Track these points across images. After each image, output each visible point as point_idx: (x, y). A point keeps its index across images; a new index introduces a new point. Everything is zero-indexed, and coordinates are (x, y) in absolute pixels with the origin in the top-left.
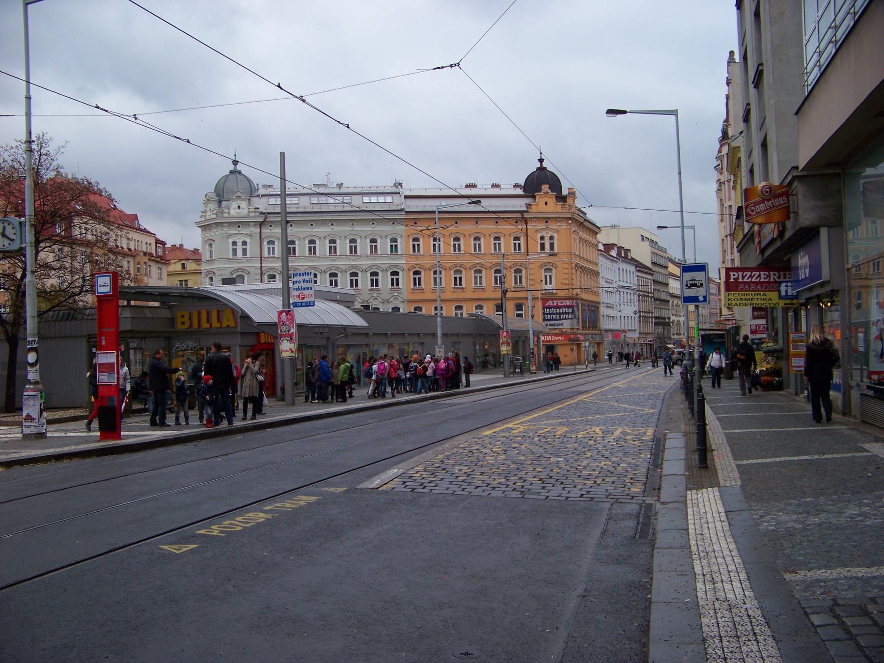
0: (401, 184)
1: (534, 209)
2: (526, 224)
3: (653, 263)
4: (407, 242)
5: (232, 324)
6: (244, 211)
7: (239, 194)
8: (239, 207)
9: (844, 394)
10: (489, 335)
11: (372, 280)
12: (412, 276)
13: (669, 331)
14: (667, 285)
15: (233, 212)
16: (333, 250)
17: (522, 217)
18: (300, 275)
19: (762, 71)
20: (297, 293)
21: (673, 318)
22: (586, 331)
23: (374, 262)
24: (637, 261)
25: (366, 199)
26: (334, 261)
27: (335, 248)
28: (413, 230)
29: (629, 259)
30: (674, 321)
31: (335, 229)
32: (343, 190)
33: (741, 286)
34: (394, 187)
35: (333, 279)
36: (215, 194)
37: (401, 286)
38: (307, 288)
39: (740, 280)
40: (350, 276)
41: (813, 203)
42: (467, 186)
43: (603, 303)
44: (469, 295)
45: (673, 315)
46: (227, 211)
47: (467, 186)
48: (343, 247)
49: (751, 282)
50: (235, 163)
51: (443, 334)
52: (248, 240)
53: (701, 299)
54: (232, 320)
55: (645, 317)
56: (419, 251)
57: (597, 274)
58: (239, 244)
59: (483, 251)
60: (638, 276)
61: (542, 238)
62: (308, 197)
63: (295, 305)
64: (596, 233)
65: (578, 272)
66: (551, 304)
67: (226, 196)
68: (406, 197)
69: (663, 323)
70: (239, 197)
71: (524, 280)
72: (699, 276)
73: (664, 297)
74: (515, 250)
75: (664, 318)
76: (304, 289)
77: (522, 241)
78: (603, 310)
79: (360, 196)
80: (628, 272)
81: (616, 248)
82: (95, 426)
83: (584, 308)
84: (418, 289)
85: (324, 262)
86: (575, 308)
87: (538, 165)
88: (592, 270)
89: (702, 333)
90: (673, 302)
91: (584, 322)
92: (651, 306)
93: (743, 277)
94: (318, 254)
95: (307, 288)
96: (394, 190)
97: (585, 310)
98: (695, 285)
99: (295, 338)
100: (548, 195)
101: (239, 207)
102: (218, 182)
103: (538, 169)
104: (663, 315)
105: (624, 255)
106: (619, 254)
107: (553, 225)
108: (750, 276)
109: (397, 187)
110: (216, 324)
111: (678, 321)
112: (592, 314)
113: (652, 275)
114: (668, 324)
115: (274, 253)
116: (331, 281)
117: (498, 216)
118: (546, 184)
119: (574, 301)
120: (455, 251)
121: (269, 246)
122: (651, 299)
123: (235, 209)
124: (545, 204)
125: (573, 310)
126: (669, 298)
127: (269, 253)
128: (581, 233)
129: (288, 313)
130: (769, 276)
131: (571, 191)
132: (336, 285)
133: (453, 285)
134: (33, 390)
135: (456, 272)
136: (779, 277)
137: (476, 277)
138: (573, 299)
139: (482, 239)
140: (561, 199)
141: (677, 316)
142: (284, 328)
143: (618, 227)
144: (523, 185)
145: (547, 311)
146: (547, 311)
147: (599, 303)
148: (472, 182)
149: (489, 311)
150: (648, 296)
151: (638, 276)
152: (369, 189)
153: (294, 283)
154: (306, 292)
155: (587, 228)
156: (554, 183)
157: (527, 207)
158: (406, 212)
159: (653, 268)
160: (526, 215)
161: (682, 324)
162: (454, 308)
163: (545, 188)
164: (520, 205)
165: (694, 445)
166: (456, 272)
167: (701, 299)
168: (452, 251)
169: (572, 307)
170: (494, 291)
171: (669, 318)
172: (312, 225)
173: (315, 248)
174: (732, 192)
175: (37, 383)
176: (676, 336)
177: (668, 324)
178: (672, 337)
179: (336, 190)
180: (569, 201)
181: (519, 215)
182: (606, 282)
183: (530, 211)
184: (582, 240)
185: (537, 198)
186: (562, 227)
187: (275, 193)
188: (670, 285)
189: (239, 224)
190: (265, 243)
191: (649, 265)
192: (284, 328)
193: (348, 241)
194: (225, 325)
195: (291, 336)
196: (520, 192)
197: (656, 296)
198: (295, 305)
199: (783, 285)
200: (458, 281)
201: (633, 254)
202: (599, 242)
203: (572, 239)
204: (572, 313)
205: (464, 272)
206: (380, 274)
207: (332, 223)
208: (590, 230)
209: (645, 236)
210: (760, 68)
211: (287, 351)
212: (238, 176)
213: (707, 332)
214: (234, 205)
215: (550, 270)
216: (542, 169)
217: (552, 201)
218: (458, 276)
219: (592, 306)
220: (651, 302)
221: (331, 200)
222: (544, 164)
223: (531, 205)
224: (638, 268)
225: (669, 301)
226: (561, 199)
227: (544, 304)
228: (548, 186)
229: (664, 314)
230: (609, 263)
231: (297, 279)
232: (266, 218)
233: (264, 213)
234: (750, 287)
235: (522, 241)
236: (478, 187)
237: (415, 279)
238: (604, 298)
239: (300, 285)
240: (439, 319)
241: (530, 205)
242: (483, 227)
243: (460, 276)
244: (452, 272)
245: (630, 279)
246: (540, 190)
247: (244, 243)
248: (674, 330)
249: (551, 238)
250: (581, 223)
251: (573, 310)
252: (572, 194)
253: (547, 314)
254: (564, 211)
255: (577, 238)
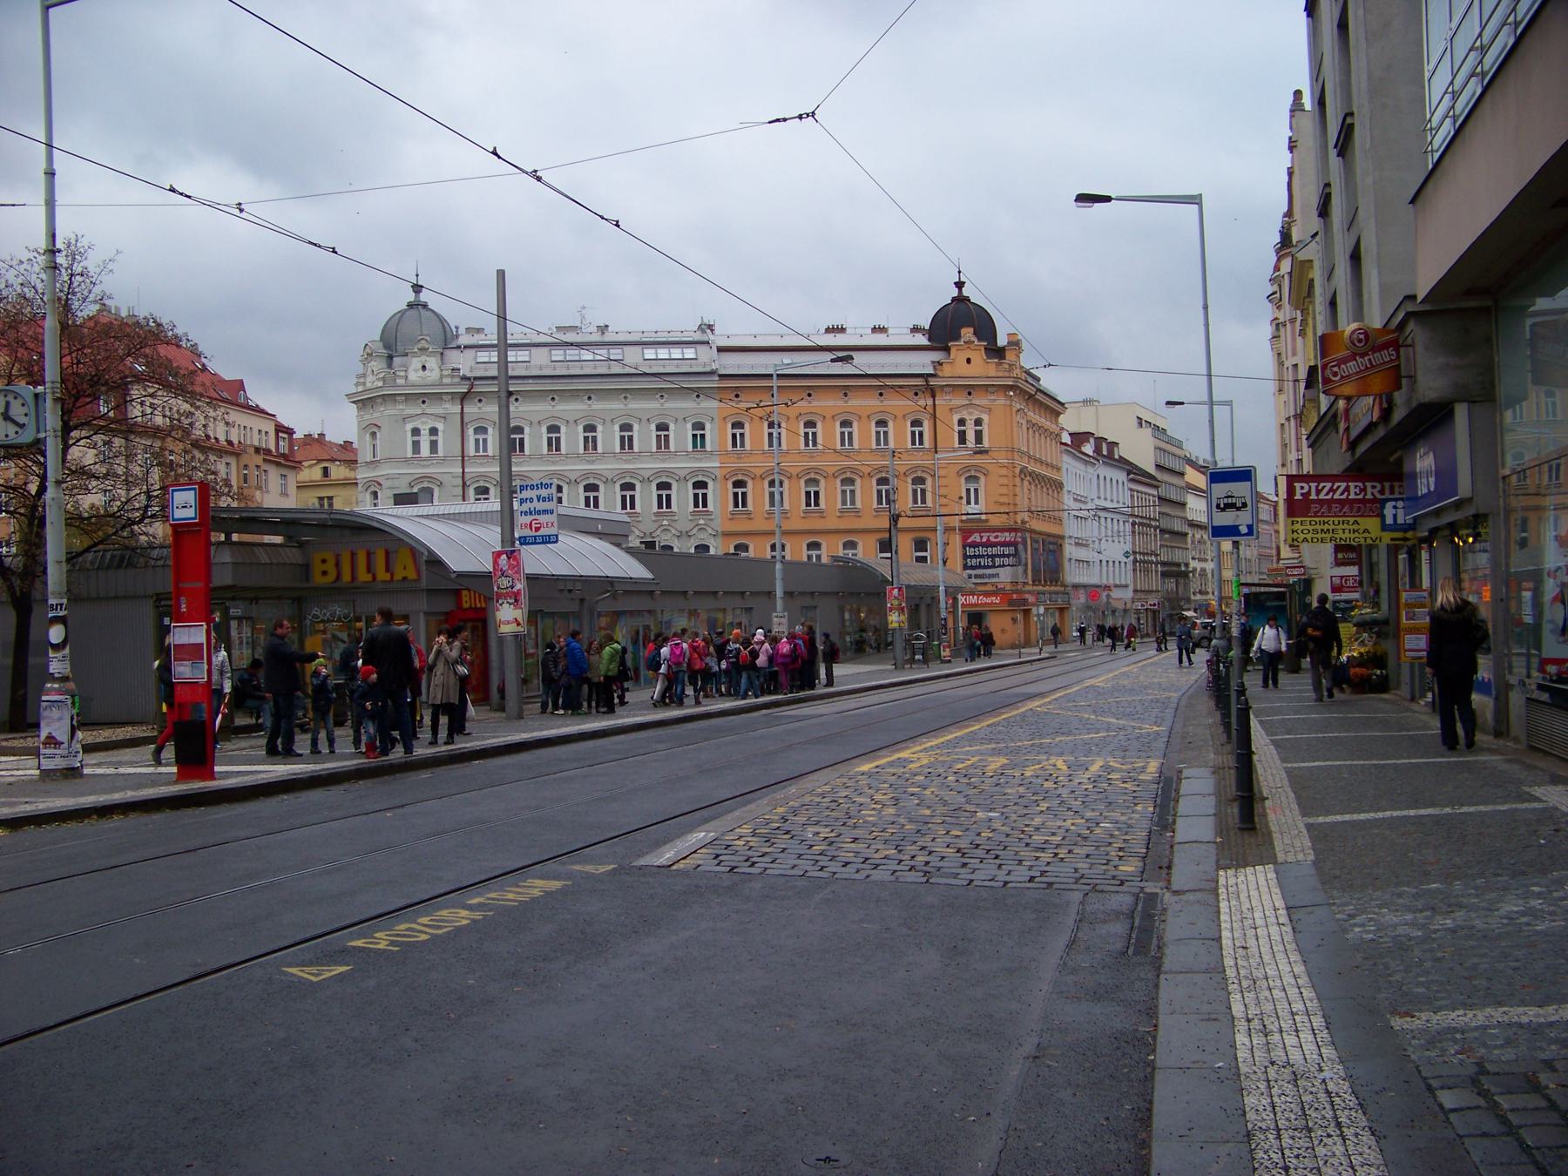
0: (710, 327)
1: (947, 371)
2: (934, 396)
3: (1158, 467)
4: (722, 430)
5: (411, 574)
6: (433, 374)
7: (423, 344)
8: (424, 367)
9: (1496, 699)
10: (868, 594)
11: (660, 497)
12: (731, 490)
13: (1186, 586)
14: (1183, 505)
15: (414, 376)
16: (590, 443)
17: (926, 386)
18: (532, 487)
19: (1351, 126)
20: (527, 519)
21: (1193, 564)
22: (1040, 588)
23: (663, 465)
24: (1130, 464)
25: (650, 353)
26: (592, 462)
27: (594, 439)
28: (732, 408)
29: (1116, 460)
30: (1195, 570)
31: (594, 407)
32: (609, 337)
33: (1314, 507)
34: (699, 333)
35: (591, 495)
36: (381, 344)
37: (710, 507)
38: (545, 512)
39: (1313, 497)
40: (622, 490)
41: (1442, 360)
42: (828, 330)
43: (1070, 537)
44: (832, 523)
45: (1193, 558)
46: (402, 374)
47: (828, 330)
48: (609, 438)
49: (1332, 501)
50: (417, 288)
51: (785, 593)
52: (440, 426)
53: (1244, 530)
54: (411, 567)
55: (1144, 562)
56: (742, 445)
57: (1059, 486)
58: (425, 432)
59: (856, 445)
60: (1131, 490)
61: (962, 422)
62: (547, 349)
63: (524, 541)
64: (1058, 414)
65: (1026, 483)
66: (978, 540)
67: (400, 348)
68: (721, 350)
69: (1176, 572)
70: (423, 350)
71: (929, 496)
72: (1239, 489)
73: (1178, 526)
74: (913, 443)
75: (1179, 565)
76: (539, 513)
77: (926, 428)
78: (1070, 550)
79: (638, 348)
80: (1114, 482)
81: (1092, 440)
82: (169, 756)
83: (1036, 546)
84: (742, 513)
85: (574, 465)
86: (1020, 547)
87: (955, 293)
88: (1050, 479)
89: (1246, 590)
90: (1193, 535)
91: (1036, 571)
92: (1154, 543)
93: (1318, 492)
94: (563, 450)
95: (545, 512)
96: (698, 337)
97: (1037, 549)
98: (1232, 506)
99: (524, 599)
100: (972, 346)
101: (424, 367)
102: (387, 322)
103: (954, 299)
104: (1176, 560)
105: (1107, 452)
106: (1098, 450)
107: (980, 400)
108: (1331, 490)
109: (704, 332)
110: (382, 575)
111: (1203, 570)
112: (1051, 557)
113: (1156, 487)
114: (1185, 575)
115: (485, 450)
116: (587, 499)
117: (883, 384)
118: (968, 326)
119: (1019, 534)
120: (807, 444)
121: (477, 437)
122: (1155, 530)
123: (416, 371)
124: (967, 361)
125: (1016, 550)
126: (1186, 529)
127: (477, 450)
128: (1030, 414)
129: (511, 555)
130: (1364, 490)
131: (1013, 339)
132: (596, 505)
133: (803, 506)
134: (59, 692)
135: (808, 482)
136: (1382, 492)
137: (844, 492)
138: (1015, 530)
139: (855, 425)
140: (996, 352)
141: (1200, 560)
142: (504, 582)
143: (1096, 403)
144: (927, 327)
145: (970, 551)
146: (970, 551)
147: (1062, 537)
148: (837, 322)
149: (867, 552)
150: (1149, 526)
151: (1131, 490)
152: (654, 335)
153: (522, 501)
154: (543, 519)
155: (1041, 404)
156: (983, 324)
157: (935, 368)
158: (720, 376)
159: (1159, 476)
160: (933, 382)
161: (1210, 575)
162: (805, 547)
163: (967, 333)
164: (922, 363)
165: (1232, 789)
166: (808, 482)
167: (1244, 530)
168: (802, 446)
169: (1014, 544)
170: (876, 516)
171: (1187, 565)
172: (553, 399)
173: (558, 439)
174: (1299, 340)
175: (65, 679)
176: (1198, 597)
177: (1185, 575)
178: (1192, 597)
179: (596, 338)
180: (1010, 356)
181: (920, 382)
182: (1075, 500)
183: (940, 374)
184: (1032, 425)
185: (953, 351)
186: (997, 402)
187: (488, 342)
188: (1188, 506)
189: (424, 398)
190: (471, 431)
191: (1151, 470)
192: (504, 582)
193: (617, 428)
194: (398, 576)
195: (516, 597)
196: (922, 340)
197: (1163, 526)
198: (524, 541)
199: (1389, 505)
200: (813, 498)
201: (1123, 451)
202: (1062, 429)
203: (1015, 424)
204: (1014, 556)
205: (822, 482)
206: (674, 486)
207: (589, 395)
208: (1047, 408)
209: (1144, 418)
210: (1349, 120)
211: (508, 623)
212: (423, 312)
213: (1254, 589)
214: (416, 363)
215: (975, 479)
216: (961, 300)
217: (978, 356)
218: (812, 490)
219: (1050, 543)
220: (1155, 536)
221: (587, 355)
222: (966, 291)
223: (941, 364)
224: (1132, 476)
225: (1186, 534)
226: (996, 352)
227: (964, 539)
228: (972, 330)
229: (1178, 556)
230: (1080, 466)
231: (526, 494)
232: (472, 386)
233: (469, 379)
234: (1330, 508)
235: (926, 428)
236: (848, 331)
237: (736, 495)
238: (1071, 529)
239: (532, 506)
240: (778, 566)
241: (940, 364)
242: (856, 403)
243: (816, 489)
244: (802, 482)
245: (1118, 495)
246: (958, 337)
247: (434, 431)
248: (1195, 585)
249: (978, 422)
250: (1031, 396)
251: (1016, 550)
252: (1015, 344)
253: (971, 557)
254: (1000, 374)
255: (1024, 422)
